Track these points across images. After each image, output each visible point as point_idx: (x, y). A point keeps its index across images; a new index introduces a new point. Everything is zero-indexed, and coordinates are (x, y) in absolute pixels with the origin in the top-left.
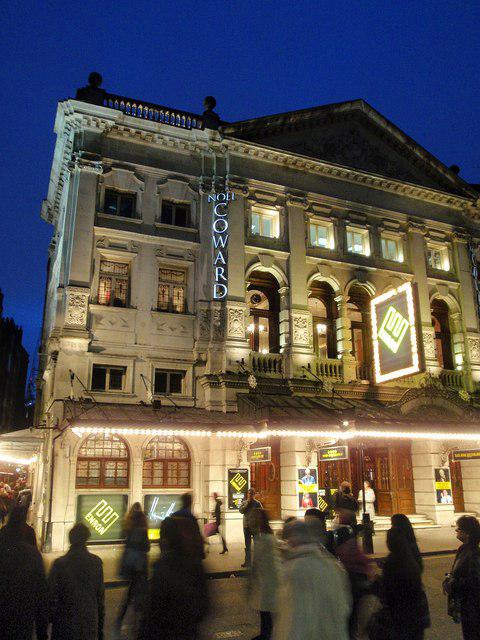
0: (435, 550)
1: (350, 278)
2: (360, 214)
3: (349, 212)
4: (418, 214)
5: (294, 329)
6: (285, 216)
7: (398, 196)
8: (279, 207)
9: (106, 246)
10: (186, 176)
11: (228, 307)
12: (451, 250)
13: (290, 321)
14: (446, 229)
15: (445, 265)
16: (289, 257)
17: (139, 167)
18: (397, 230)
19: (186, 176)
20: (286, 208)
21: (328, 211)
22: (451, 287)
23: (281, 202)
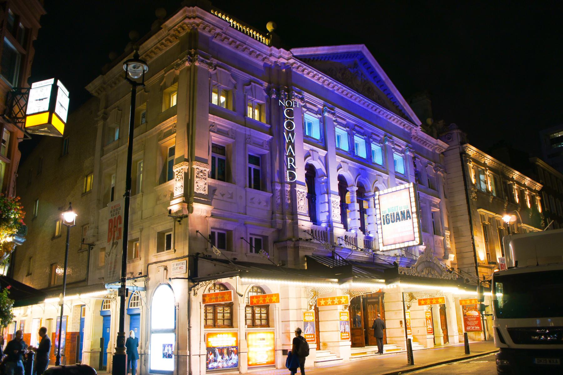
0: (426, 365)
1: (356, 175)
2: (361, 128)
3: (356, 125)
4: (391, 132)
5: (332, 209)
6: (323, 121)
7: (380, 117)
8: (347, 129)
9: (216, 131)
10: (261, 81)
11: (297, 189)
12: (405, 159)
13: (329, 202)
14: (403, 145)
15: (400, 169)
16: (326, 155)
17: (234, 69)
18: (316, 113)
19: (261, 81)
20: (385, 146)
21: (344, 122)
22: (320, 154)
23: (320, 112)
